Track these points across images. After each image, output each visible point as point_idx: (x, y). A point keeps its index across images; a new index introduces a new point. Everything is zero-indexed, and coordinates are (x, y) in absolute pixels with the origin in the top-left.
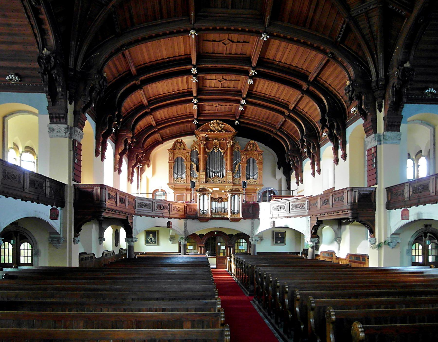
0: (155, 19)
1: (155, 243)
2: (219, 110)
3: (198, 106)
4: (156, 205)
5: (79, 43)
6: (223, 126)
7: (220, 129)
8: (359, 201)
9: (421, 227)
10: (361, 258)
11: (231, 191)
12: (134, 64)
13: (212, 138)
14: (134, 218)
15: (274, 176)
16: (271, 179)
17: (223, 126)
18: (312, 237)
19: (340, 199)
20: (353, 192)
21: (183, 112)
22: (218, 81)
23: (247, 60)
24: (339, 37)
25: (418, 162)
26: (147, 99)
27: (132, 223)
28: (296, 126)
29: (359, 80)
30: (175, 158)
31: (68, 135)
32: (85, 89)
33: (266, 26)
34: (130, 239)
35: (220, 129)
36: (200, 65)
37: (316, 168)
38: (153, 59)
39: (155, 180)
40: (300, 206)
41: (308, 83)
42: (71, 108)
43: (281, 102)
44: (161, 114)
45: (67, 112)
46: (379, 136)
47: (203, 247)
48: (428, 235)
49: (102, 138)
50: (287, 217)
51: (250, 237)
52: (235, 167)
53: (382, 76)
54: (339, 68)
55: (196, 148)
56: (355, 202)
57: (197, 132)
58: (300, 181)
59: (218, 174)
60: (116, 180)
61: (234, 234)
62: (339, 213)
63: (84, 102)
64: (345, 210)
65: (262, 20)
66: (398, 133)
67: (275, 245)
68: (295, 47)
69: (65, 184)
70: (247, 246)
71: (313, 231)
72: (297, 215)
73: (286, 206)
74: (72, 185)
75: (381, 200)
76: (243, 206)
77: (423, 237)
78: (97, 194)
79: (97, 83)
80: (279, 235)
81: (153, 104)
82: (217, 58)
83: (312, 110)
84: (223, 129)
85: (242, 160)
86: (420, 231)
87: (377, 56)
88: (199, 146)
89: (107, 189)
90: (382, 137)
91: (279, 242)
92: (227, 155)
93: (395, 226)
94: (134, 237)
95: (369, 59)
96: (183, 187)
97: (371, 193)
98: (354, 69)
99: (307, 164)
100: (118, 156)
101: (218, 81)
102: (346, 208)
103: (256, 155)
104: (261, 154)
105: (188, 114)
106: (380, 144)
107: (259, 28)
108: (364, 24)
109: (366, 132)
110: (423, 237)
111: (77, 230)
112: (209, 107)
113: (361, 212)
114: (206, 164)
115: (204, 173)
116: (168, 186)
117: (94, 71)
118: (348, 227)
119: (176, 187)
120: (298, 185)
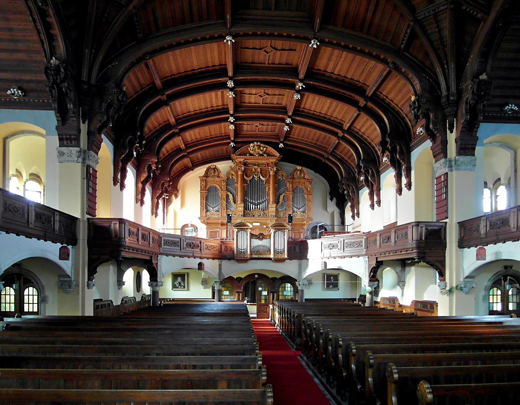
0: (184, 23)
1: (184, 287)
2: (260, 130)
3: (235, 126)
4: (185, 243)
5: (93, 51)
6: (265, 149)
7: (261, 152)
8: (426, 238)
9: (499, 268)
10: (429, 306)
11: (274, 226)
12: (159, 76)
13: (251, 164)
14: (159, 258)
15: (326, 208)
16: (322, 212)
17: (265, 149)
18: (370, 281)
19: (404, 235)
20: (419, 228)
21: (218, 133)
22: (259, 96)
23: (294, 71)
24: (402, 43)
25: (496, 192)
26: (174, 117)
27: (157, 264)
28: (351, 149)
29: (426, 95)
30: (207, 188)
31: (80, 160)
32: (101, 105)
33: (316, 31)
34: (154, 284)
35: (261, 152)
36: (237, 77)
37: (376, 199)
38: (182, 70)
39: (184, 213)
40: (357, 244)
41: (366, 98)
42: (84, 127)
43: (334, 121)
44: (191, 135)
45: (80, 133)
46: (450, 161)
47: (241, 292)
48: (508, 278)
49: (121, 164)
50: (341, 257)
51: (296, 281)
52: (279, 197)
53: (453, 90)
54: (403, 81)
55: (232, 175)
56: (421, 239)
57: (233, 156)
58: (356, 215)
59: (259, 206)
60: (138, 213)
61: (278, 277)
62: (403, 253)
63: (100, 121)
64: (410, 248)
65: (311, 24)
66: (473, 157)
67: (326, 290)
68: (351, 55)
69: (77, 218)
70: (294, 291)
71: (372, 274)
72: (352, 254)
73: (339, 244)
74: (85, 219)
75: (452, 237)
76: (288, 244)
77: (503, 281)
78: (115, 230)
79: (115, 98)
80: (331, 278)
81: (181, 123)
82: (258, 68)
83: (371, 130)
84: (265, 153)
85: (287, 190)
86: (499, 274)
87: (448, 66)
88: (237, 173)
89: (126, 224)
90: (454, 162)
91: (331, 286)
92: (269, 183)
93: (468, 267)
94: (159, 280)
95: (439, 70)
96: (217, 222)
97: (440, 229)
98: (421, 81)
99: (364, 194)
100: (140, 185)
101: (259, 96)
102: (410, 246)
103: (304, 183)
104: (310, 183)
105: (223, 135)
106: (452, 171)
107: (308, 33)
108: (432, 29)
109: (434, 157)
110: (503, 281)
111: (92, 272)
112: (248, 127)
113: (429, 251)
114: (245, 194)
115: (243, 205)
116: (199, 221)
117: (111, 84)
118: (413, 269)
119: (209, 221)
120: (354, 219)
